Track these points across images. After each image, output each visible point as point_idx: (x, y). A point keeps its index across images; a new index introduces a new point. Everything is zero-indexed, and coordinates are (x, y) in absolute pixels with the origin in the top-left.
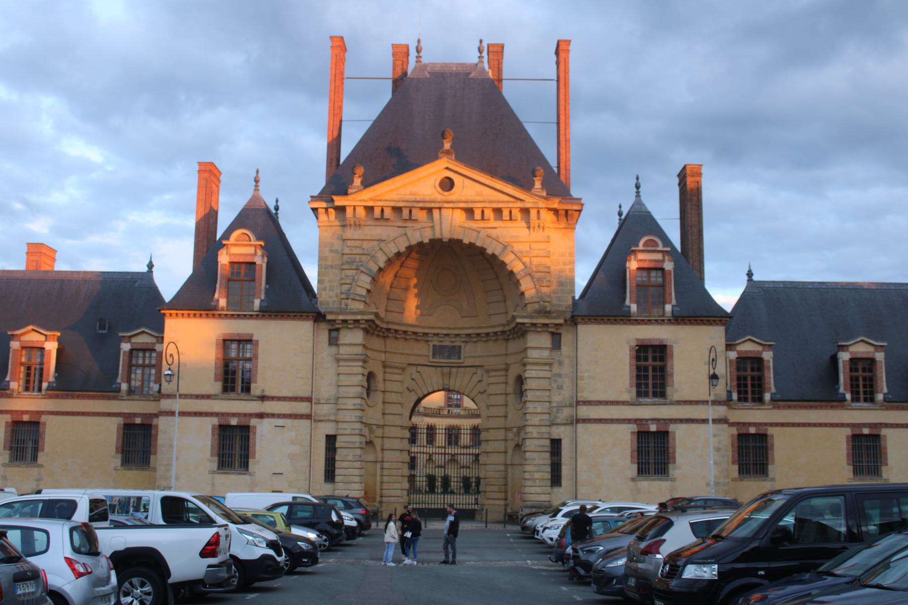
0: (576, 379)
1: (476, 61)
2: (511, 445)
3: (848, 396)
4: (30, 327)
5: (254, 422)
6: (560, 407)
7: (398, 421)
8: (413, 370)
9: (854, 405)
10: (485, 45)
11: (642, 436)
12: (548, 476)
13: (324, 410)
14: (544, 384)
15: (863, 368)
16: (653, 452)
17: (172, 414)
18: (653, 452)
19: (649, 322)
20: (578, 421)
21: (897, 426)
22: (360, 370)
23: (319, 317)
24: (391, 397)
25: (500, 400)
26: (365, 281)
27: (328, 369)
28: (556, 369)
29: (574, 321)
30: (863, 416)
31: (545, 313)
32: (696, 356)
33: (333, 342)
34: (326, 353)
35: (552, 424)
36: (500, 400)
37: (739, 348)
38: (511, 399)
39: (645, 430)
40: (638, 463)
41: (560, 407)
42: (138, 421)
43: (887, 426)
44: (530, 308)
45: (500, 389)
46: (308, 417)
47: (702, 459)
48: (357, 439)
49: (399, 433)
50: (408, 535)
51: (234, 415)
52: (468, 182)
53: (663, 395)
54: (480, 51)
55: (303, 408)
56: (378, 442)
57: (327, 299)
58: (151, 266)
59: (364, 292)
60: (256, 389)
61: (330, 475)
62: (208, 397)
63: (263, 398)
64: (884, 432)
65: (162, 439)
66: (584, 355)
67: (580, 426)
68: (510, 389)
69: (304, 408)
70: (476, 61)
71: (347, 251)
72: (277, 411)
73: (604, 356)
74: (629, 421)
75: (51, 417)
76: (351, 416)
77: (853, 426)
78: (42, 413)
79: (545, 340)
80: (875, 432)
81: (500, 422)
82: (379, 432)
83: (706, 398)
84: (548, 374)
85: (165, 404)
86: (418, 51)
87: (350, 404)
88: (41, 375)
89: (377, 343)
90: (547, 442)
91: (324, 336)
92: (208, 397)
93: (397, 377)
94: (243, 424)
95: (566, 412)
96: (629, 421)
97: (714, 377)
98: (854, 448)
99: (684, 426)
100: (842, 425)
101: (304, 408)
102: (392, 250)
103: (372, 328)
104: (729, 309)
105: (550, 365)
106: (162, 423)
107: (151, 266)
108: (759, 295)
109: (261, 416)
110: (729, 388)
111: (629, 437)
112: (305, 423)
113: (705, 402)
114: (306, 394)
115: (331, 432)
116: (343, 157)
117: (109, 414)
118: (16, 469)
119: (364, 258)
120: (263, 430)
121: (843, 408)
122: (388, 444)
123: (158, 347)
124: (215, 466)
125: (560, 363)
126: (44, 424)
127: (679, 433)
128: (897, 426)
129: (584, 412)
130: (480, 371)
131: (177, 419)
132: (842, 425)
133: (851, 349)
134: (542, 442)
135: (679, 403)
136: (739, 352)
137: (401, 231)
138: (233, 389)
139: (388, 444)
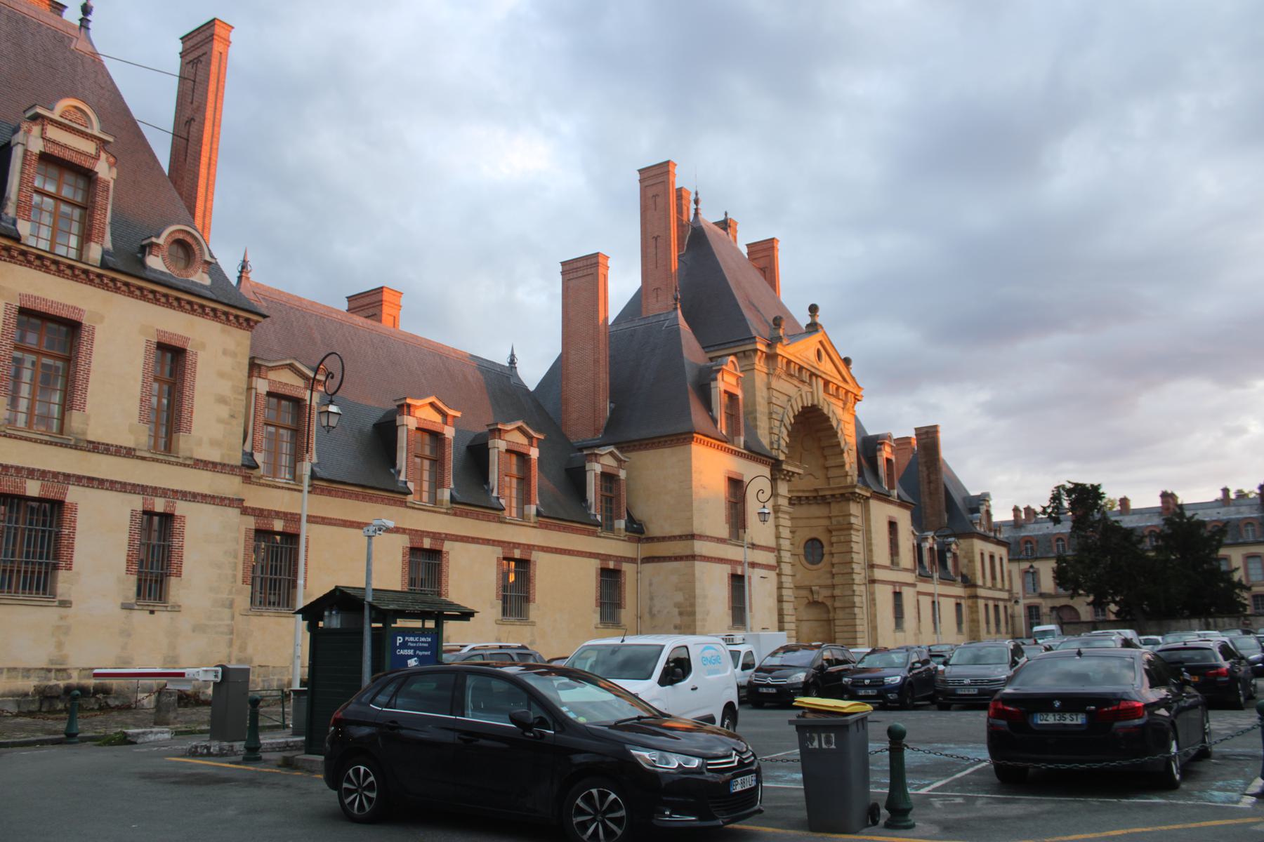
4: (611, 448)
39: (17, 491)
40: (139, 573)
50: (1057, 704)
51: (31, 473)
62: (129, 453)
63: (753, 546)
75: (541, 554)
92: (129, 453)
94: (51, 495)
104: (532, 387)
109: (753, 565)
110: (248, 448)
118: (510, 628)
126: (74, 508)
133: (508, 437)
136: (271, 382)
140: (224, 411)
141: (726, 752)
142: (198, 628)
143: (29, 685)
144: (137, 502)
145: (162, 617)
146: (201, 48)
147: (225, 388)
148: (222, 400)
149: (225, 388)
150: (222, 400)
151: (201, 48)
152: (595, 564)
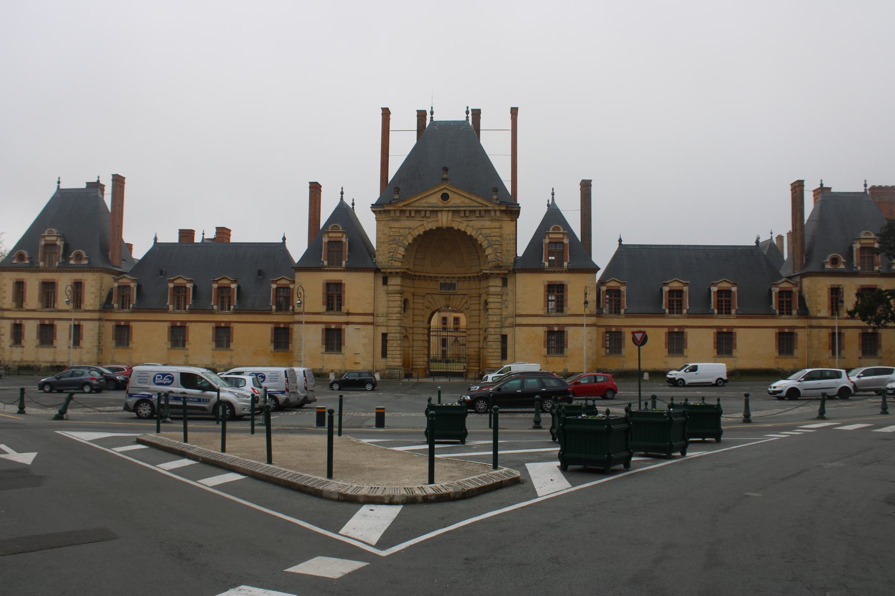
0: (515, 302)
1: (465, 119)
2: (482, 338)
3: (716, 311)
5: (343, 327)
6: (506, 318)
7: (421, 324)
8: (429, 297)
9: (670, 316)
10: (470, 110)
11: (550, 333)
12: (500, 354)
13: (381, 320)
14: (498, 305)
15: (724, 294)
16: (556, 340)
17: (301, 323)
18: (556, 340)
19: (555, 272)
20: (516, 325)
21: (693, 327)
22: (399, 298)
23: (377, 271)
24: (417, 312)
25: (477, 313)
26: (402, 250)
27: (383, 298)
28: (505, 297)
29: (514, 271)
30: (785, 322)
31: (499, 267)
32: (579, 290)
33: (385, 282)
34: (382, 289)
35: (502, 327)
36: (477, 313)
37: (608, 284)
38: (482, 312)
41: (506, 318)
42: (282, 326)
43: (687, 327)
44: (490, 265)
45: (477, 307)
46: (372, 324)
47: (583, 343)
48: (398, 335)
49: (421, 331)
51: (333, 323)
52: (456, 196)
53: (562, 311)
54: (467, 113)
55: (369, 319)
56: (410, 337)
57: (381, 259)
58: (284, 239)
59: (401, 257)
60: (344, 309)
61: (384, 354)
63: (348, 314)
64: (686, 330)
65: (295, 336)
66: (520, 289)
67: (517, 328)
68: (482, 307)
69: (371, 319)
70: (465, 119)
71: (392, 234)
72: (638, 324)
73: (530, 291)
74: (773, 327)
76: (396, 323)
77: (669, 327)
78: (735, 327)
79: (499, 282)
80: (681, 330)
81: (476, 325)
82: (410, 331)
83: (583, 313)
84: (500, 300)
85: (297, 318)
86: (432, 113)
87: (394, 317)
88: (229, 302)
89: (409, 282)
90: (499, 337)
91: (380, 281)
93: (421, 301)
95: (510, 320)
96: (543, 325)
97: (586, 302)
98: (669, 339)
99: (572, 328)
100: (663, 327)
101: (371, 319)
102: (416, 233)
103: (404, 275)
105: (501, 295)
106: (296, 327)
107: (284, 239)
108: (627, 255)
109: (347, 323)
111: (543, 334)
112: (371, 327)
113: (582, 315)
114: (372, 312)
115: (385, 331)
116: (390, 178)
117: (266, 323)
119: (401, 238)
120: (349, 331)
121: (712, 318)
122: (416, 337)
123: (291, 286)
124: (324, 350)
125: (507, 294)
127: (570, 331)
128: (693, 327)
129: (519, 320)
130: (466, 297)
131: (304, 326)
132: (663, 327)
134: (496, 336)
135: (570, 315)
137: (421, 223)
138: (332, 309)
139: (416, 337)
140: (93, 296)
141: (711, 398)
142: (88, 352)
143: (48, 365)
144: (13, 322)
145: (78, 350)
146: (586, 187)
147: (93, 290)
148: (93, 293)
149: (93, 290)
150: (93, 293)
151: (586, 187)
152: (166, 325)
